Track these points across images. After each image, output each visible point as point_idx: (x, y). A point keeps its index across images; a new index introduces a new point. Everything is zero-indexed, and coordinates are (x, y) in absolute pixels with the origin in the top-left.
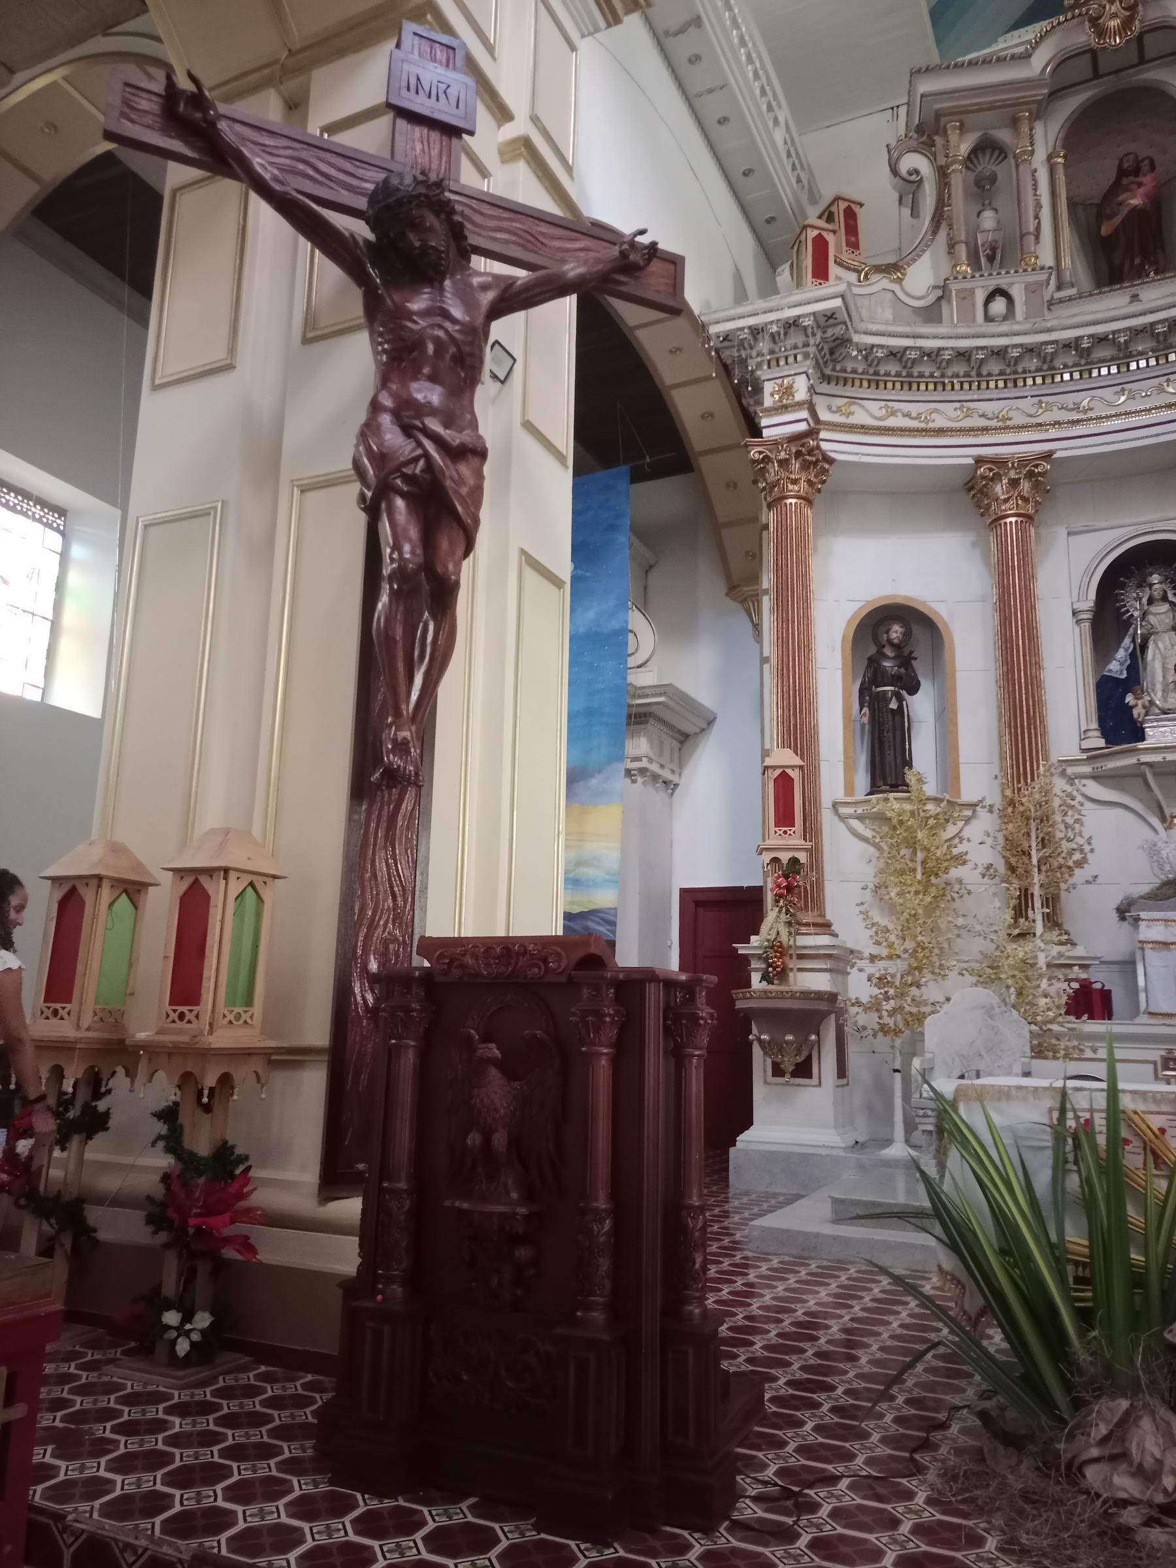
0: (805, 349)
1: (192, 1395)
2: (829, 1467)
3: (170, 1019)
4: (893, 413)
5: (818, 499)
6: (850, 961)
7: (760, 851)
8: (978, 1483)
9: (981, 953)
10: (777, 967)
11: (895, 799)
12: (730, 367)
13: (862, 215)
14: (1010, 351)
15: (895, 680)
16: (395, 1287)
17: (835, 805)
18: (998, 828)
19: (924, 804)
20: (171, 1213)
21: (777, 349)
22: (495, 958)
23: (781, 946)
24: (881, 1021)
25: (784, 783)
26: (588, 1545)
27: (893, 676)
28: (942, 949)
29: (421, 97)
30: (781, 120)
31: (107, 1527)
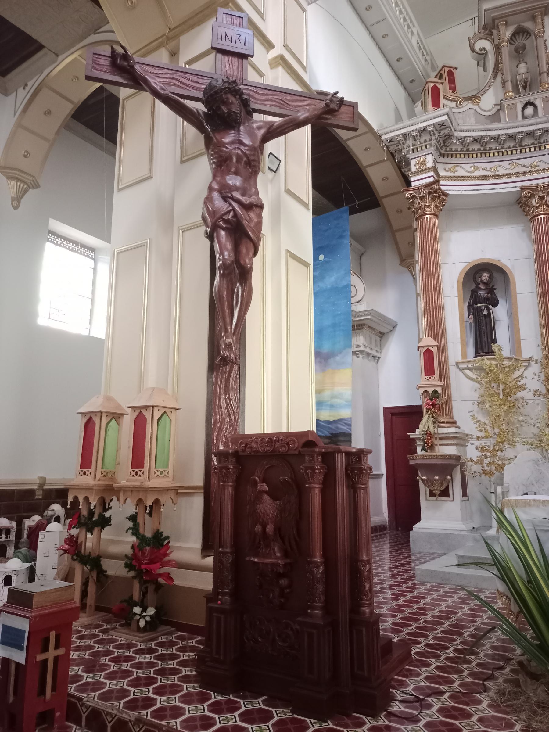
0: (431, 142)
1: (146, 645)
2: (441, 687)
3: (132, 475)
4: (477, 169)
5: (441, 214)
6: (466, 440)
7: (419, 388)
8: (515, 697)
9: (533, 433)
10: (429, 443)
11: (487, 359)
12: (394, 154)
13: (456, 73)
14: (536, 132)
15: (486, 300)
16: (227, 597)
17: (457, 364)
18: (540, 371)
19: (503, 361)
20: (134, 563)
21: (416, 144)
22: (265, 443)
23: (430, 434)
24: (483, 469)
25: (428, 355)
26: (316, 721)
27: (484, 298)
28: (513, 432)
29: (228, 43)
30: (415, 32)
31: (100, 704)
